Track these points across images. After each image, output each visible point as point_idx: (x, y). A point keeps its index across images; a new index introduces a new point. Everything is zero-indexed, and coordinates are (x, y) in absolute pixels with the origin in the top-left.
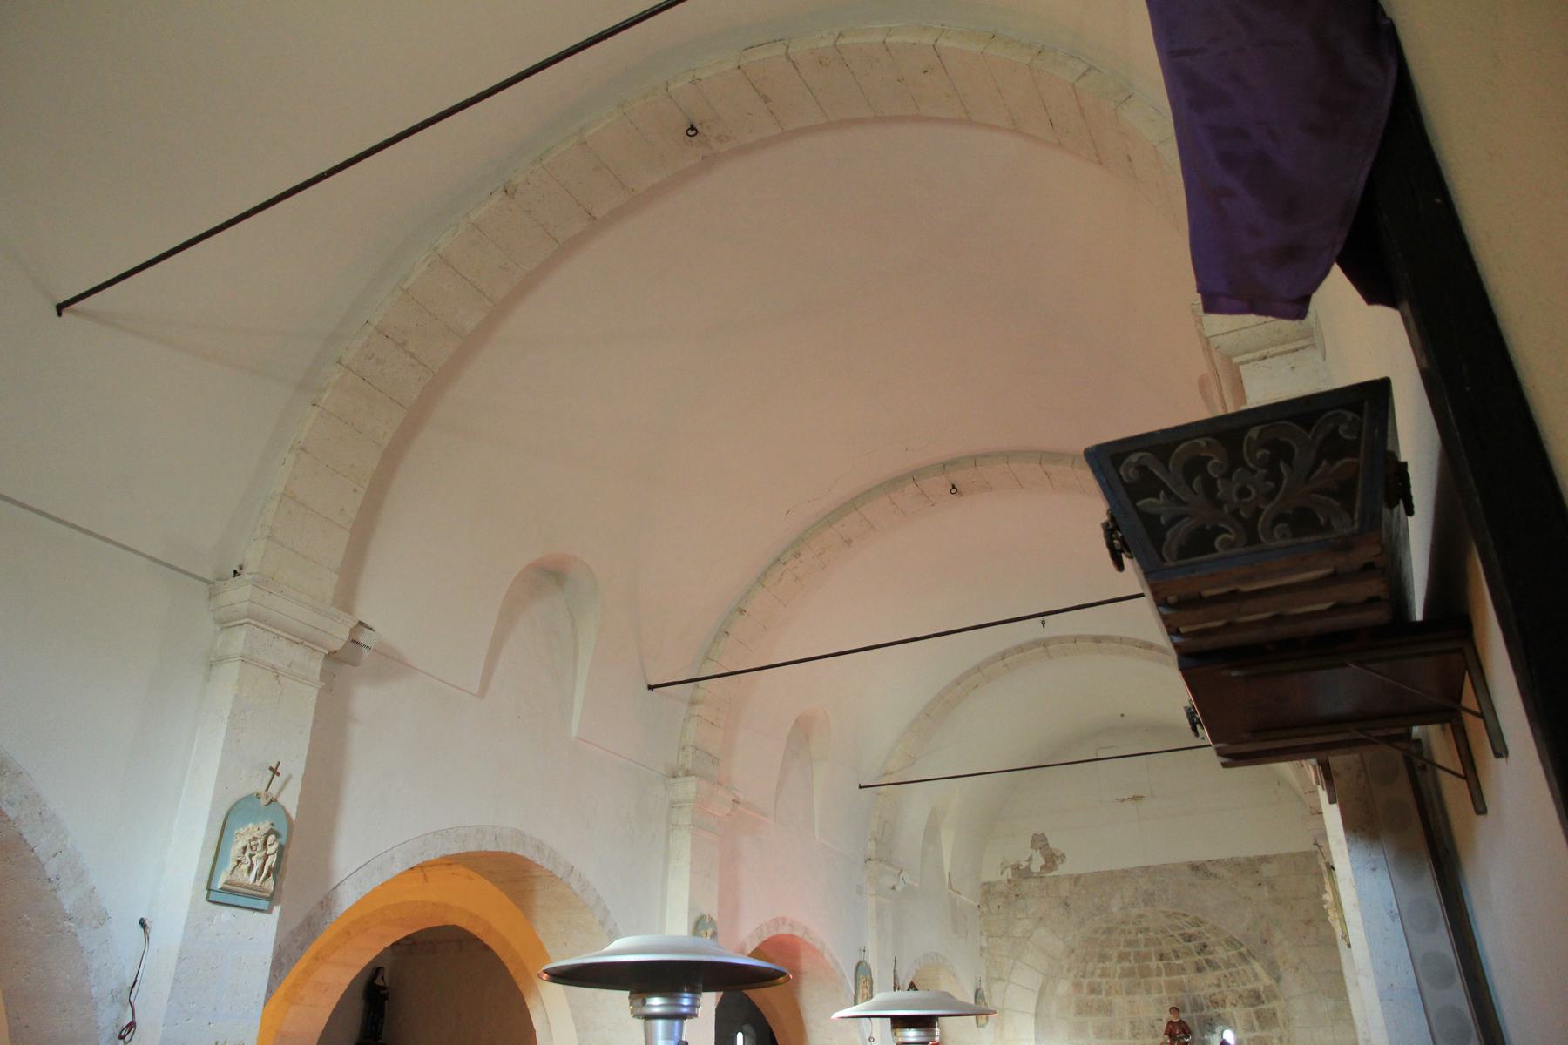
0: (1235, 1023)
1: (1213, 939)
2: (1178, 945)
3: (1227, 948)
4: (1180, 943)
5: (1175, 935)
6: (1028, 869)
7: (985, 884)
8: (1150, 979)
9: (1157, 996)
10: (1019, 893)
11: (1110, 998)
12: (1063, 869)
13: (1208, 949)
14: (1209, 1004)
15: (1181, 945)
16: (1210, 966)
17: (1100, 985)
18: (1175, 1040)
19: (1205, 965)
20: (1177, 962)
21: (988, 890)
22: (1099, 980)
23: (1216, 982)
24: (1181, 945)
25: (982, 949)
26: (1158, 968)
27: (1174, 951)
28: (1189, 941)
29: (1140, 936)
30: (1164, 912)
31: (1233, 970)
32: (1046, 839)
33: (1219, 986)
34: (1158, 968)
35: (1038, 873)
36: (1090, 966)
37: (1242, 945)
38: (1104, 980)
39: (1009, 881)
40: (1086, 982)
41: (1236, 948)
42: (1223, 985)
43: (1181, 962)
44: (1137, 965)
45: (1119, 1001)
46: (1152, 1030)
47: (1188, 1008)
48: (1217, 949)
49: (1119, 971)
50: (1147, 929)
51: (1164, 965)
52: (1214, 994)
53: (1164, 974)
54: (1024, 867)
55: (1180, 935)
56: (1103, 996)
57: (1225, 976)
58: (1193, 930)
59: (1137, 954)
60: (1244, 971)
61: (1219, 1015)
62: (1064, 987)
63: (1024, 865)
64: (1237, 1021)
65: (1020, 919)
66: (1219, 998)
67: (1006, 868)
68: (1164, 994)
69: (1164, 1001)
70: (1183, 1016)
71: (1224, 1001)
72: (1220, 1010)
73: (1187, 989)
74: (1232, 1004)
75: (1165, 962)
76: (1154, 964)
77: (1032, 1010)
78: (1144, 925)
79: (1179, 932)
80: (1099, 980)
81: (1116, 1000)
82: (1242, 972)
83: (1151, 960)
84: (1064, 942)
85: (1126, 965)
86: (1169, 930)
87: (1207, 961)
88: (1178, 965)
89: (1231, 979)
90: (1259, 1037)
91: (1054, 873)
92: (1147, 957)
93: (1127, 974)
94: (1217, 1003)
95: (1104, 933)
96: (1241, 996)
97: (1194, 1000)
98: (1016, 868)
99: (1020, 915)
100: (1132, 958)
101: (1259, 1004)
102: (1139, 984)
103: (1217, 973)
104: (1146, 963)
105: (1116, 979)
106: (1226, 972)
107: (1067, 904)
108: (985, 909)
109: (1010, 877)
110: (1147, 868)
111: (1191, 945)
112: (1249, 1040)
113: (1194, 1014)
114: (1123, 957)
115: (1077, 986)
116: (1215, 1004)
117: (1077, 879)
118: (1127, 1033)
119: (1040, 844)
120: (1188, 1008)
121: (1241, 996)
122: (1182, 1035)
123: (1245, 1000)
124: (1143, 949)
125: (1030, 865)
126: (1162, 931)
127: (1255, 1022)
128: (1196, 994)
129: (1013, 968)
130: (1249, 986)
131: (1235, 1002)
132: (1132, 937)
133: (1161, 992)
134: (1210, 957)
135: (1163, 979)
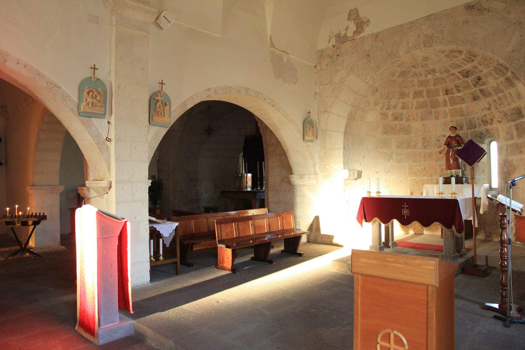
0: (499, 135)
1: (485, 71)
2: (459, 81)
3: (497, 76)
4: (461, 79)
5: (457, 73)
6: (345, 35)
7: (319, 51)
8: (439, 109)
9: (443, 120)
10: (339, 53)
11: (408, 123)
12: (368, 31)
13: (482, 81)
14: (481, 123)
15: (462, 81)
16: (483, 95)
17: (401, 114)
18: (450, 148)
19: (480, 95)
20: (459, 95)
21: (321, 55)
22: (400, 111)
23: (487, 106)
24: (462, 81)
25: (316, 94)
26: (445, 100)
27: (456, 86)
28: (467, 77)
29: (429, 77)
30: (443, 52)
31: (501, 95)
32: (358, 11)
33: (489, 109)
34: (445, 100)
35: (352, 37)
36: (393, 102)
37: (507, 69)
38: (405, 111)
39: (334, 46)
40: (391, 112)
41: (504, 74)
42: (493, 107)
43: (462, 94)
44: (428, 100)
45: (416, 125)
46: (438, 142)
47: (465, 127)
48: (488, 79)
49: (415, 104)
50: (433, 71)
51: (449, 98)
52: (485, 116)
53: (449, 104)
54: (343, 35)
55: (460, 72)
56: (404, 122)
57: (495, 101)
58: (469, 66)
59: (429, 91)
60: (510, 94)
61: (487, 131)
62: (372, 116)
63: (343, 33)
64: (500, 133)
65: (339, 71)
66: (488, 118)
67: (332, 38)
68: (449, 118)
69: (448, 123)
70: (460, 133)
71: (492, 120)
72: (489, 127)
73: (465, 114)
74: (498, 121)
75: (450, 96)
76: (441, 97)
77: (343, 130)
78: (431, 67)
79: (459, 70)
80: (400, 111)
81: (414, 124)
82: (507, 95)
83: (439, 95)
84: (366, 83)
85: (421, 100)
86: (451, 70)
87: (481, 91)
88: (459, 97)
89: (499, 102)
90: (516, 144)
91: (362, 35)
92: (436, 93)
93: (421, 106)
94: (487, 122)
95: (400, 76)
96: (506, 115)
97: (470, 121)
98: (338, 36)
99: (339, 68)
100: (425, 95)
101: (519, 119)
102: (430, 113)
103: (489, 99)
104: (435, 98)
105: (414, 110)
106: (496, 98)
107: (368, 55)
108: (319, 68)
109: (334, 43)
110: (429, 17)
111: (469, 80)
112: (507, 146)
113: (469, 131)
114: (418, 94)
115: (384, 115)
116: (485, 122)
117: (376, 36)
118: (420, 145)
119: (354, 17)
120: (465, 127)
121: (506, 115)
122: (456, 144)
123: (508, 117)
124: (432, 87)
125: (346, 32)
126: (445, 71)
127: (515, 133)
128: (471, 117)
129: (333, 104)
130: (513, 106)
131: (500, 120)
132: (422, 78)
133: (446, 117)
134: (483, 87)
135: (448, 108)
